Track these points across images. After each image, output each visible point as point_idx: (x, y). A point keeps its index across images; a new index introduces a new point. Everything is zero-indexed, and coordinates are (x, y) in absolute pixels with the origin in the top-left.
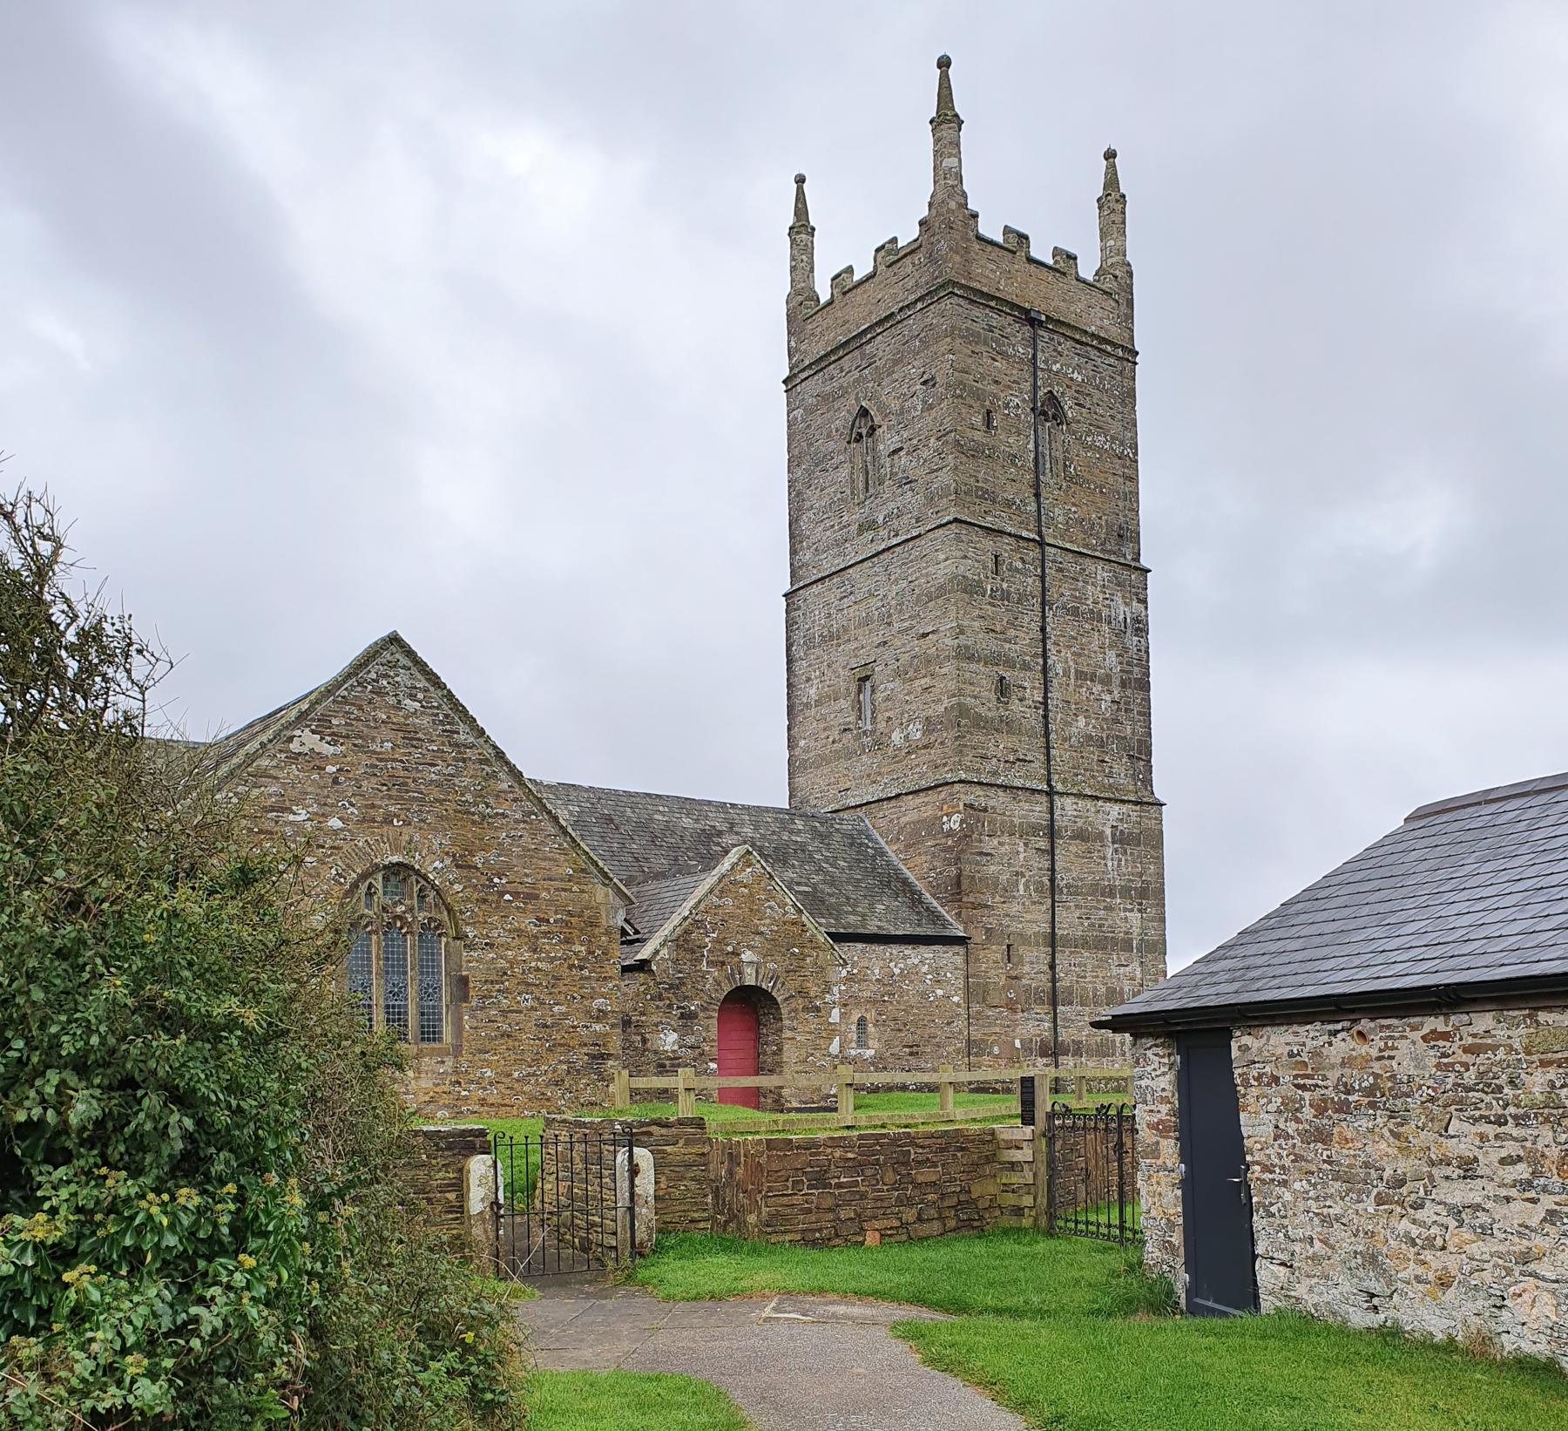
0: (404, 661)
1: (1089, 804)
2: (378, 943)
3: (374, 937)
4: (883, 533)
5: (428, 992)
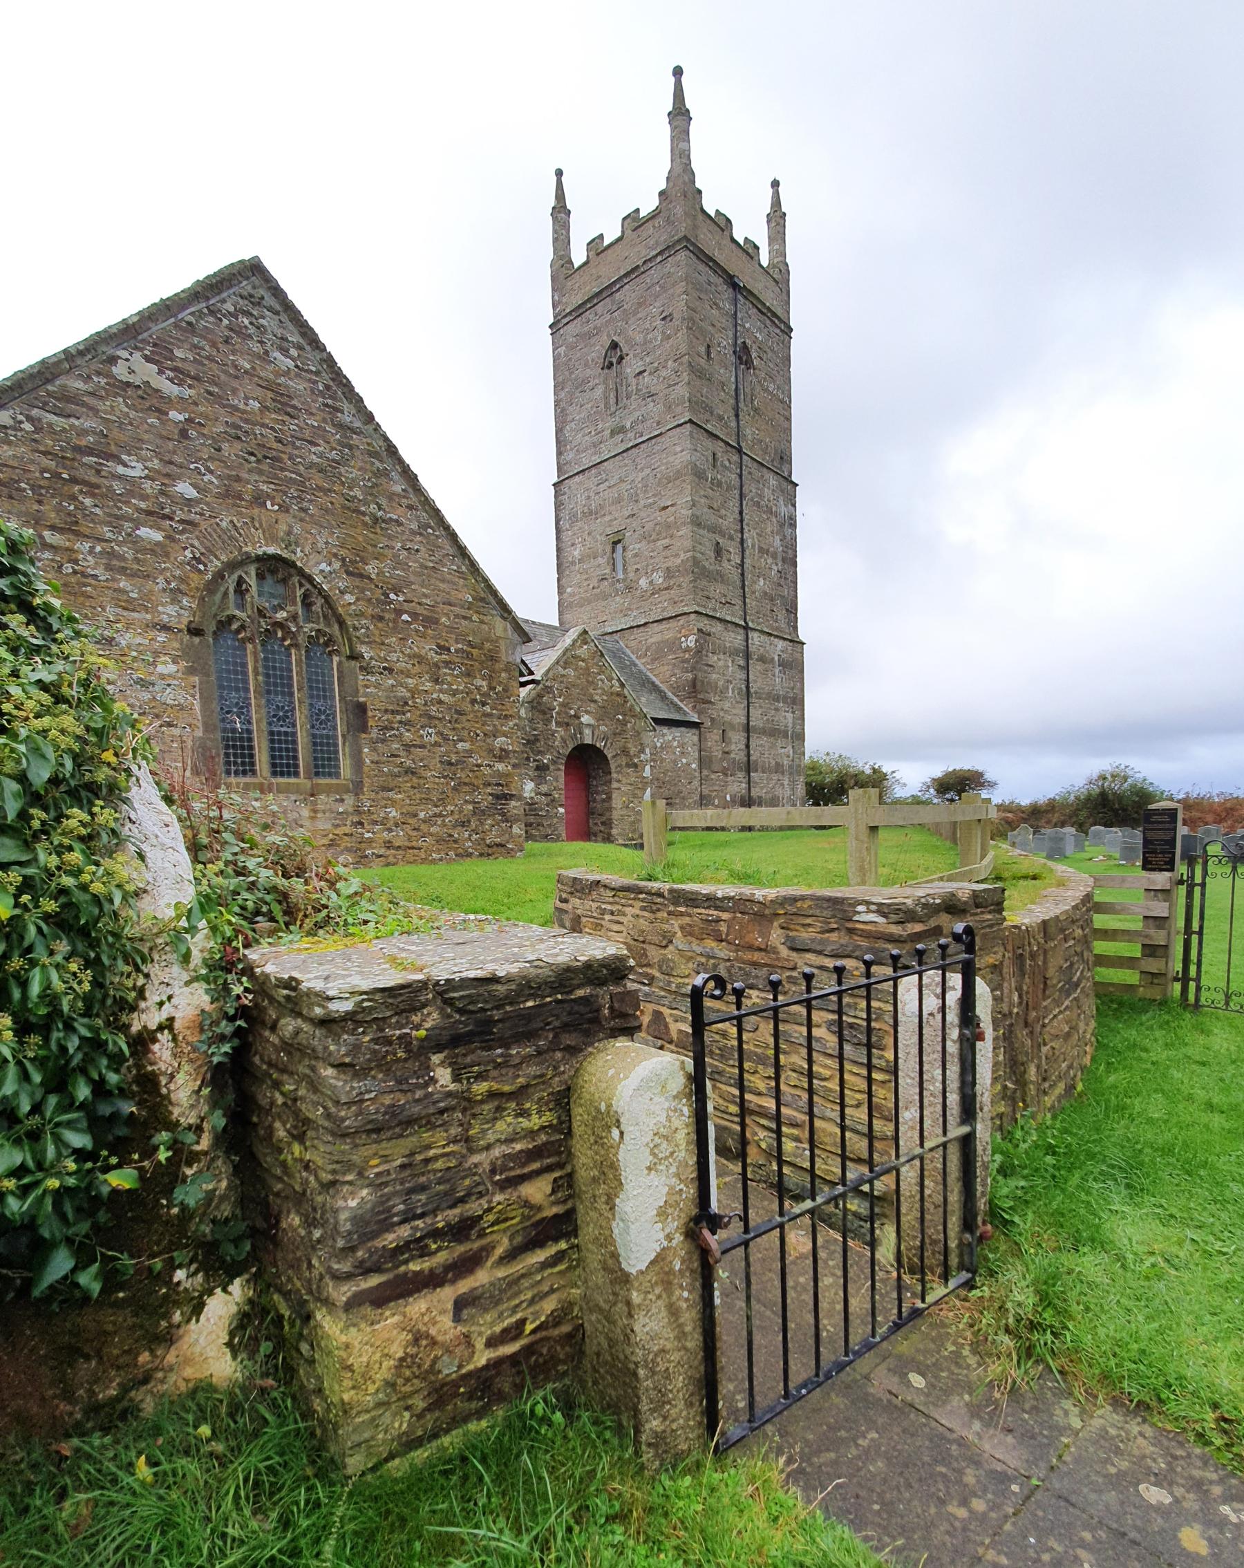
0: (269, 300)
1: (767, 638)
2: (255, 654)
3: (250, 646)
4: (630, 435)
5: (320, 718)
